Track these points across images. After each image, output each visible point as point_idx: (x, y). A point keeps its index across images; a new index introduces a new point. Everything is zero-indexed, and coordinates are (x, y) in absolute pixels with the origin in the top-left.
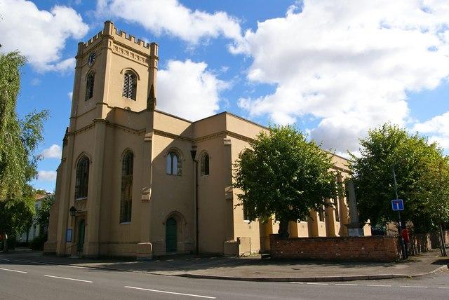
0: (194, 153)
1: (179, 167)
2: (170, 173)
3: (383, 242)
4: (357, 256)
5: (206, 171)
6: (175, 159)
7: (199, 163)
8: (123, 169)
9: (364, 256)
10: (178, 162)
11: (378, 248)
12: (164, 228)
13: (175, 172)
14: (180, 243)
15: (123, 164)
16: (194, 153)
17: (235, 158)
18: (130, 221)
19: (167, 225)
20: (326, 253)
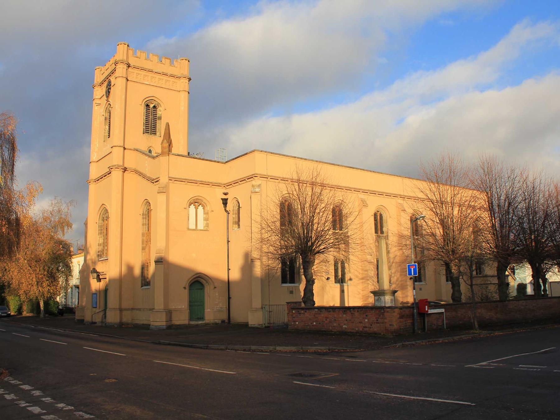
0: (225, 202)
1: (206, 219)
2: (193, 227)
3: (383, 315)
4: (361, 329)
5: (238, 223)
6: (200, 208)
7: (231, 213)
8: (143, 225)
9: (367, 329)
10: (204, 213)
11: (380, 320)
12: (186, 292)
13: (201, 226)
14: (207, 310)
15: (143, 218)
16: (225, 202)
17: (28, 315)
18: (335, 282)
19: (190, 290)
20: (335, 325)
